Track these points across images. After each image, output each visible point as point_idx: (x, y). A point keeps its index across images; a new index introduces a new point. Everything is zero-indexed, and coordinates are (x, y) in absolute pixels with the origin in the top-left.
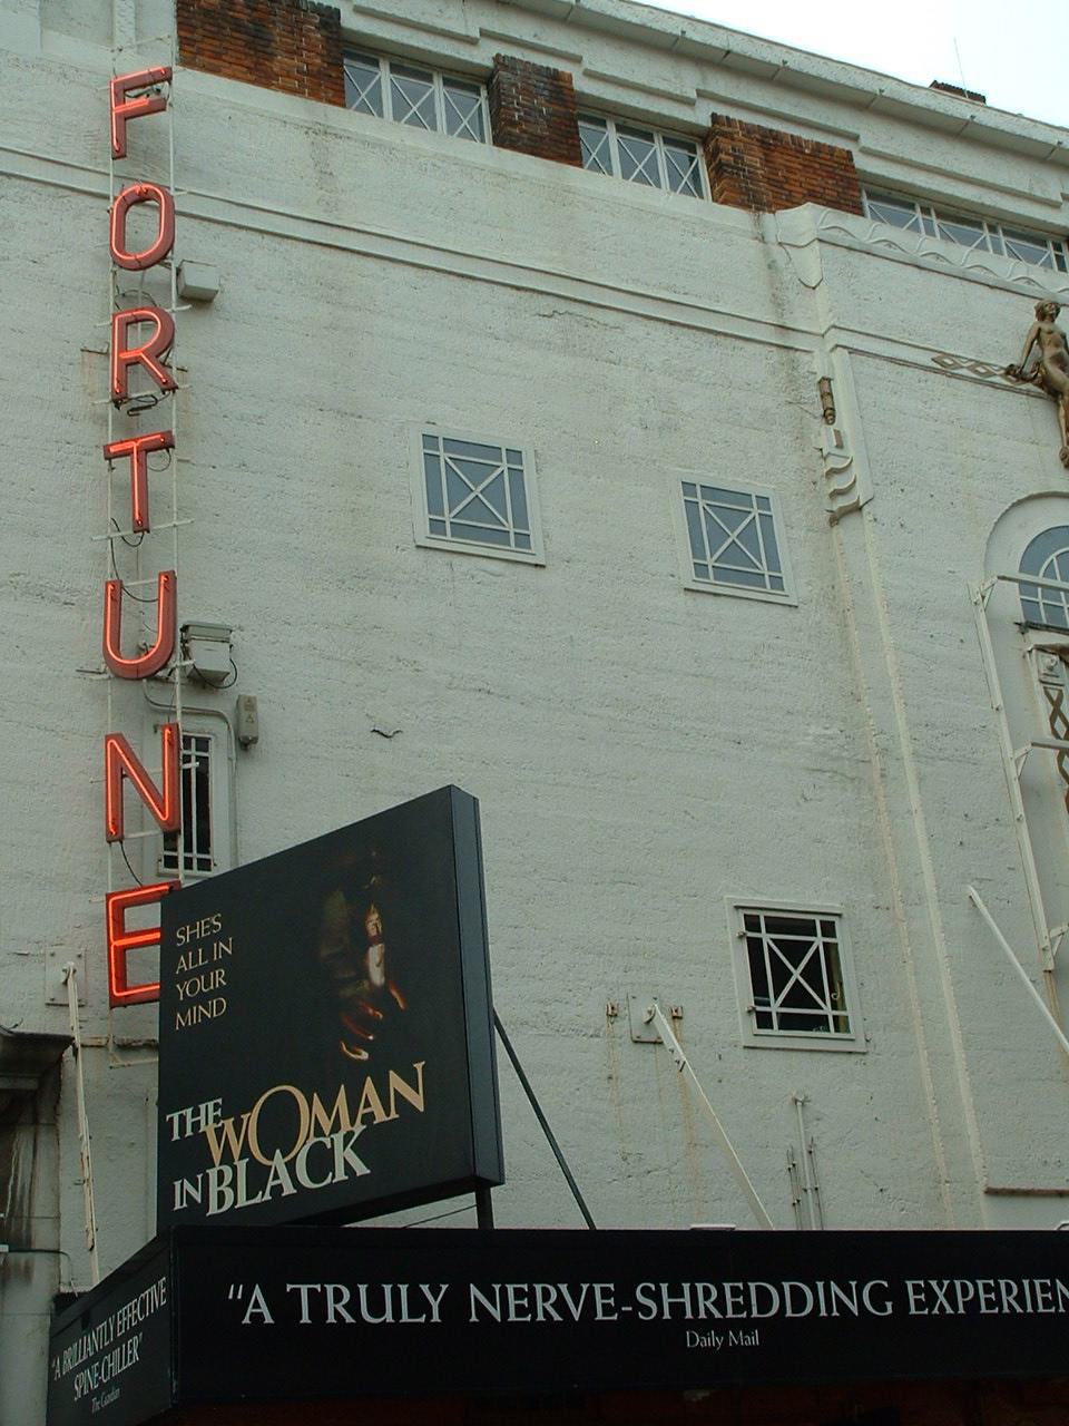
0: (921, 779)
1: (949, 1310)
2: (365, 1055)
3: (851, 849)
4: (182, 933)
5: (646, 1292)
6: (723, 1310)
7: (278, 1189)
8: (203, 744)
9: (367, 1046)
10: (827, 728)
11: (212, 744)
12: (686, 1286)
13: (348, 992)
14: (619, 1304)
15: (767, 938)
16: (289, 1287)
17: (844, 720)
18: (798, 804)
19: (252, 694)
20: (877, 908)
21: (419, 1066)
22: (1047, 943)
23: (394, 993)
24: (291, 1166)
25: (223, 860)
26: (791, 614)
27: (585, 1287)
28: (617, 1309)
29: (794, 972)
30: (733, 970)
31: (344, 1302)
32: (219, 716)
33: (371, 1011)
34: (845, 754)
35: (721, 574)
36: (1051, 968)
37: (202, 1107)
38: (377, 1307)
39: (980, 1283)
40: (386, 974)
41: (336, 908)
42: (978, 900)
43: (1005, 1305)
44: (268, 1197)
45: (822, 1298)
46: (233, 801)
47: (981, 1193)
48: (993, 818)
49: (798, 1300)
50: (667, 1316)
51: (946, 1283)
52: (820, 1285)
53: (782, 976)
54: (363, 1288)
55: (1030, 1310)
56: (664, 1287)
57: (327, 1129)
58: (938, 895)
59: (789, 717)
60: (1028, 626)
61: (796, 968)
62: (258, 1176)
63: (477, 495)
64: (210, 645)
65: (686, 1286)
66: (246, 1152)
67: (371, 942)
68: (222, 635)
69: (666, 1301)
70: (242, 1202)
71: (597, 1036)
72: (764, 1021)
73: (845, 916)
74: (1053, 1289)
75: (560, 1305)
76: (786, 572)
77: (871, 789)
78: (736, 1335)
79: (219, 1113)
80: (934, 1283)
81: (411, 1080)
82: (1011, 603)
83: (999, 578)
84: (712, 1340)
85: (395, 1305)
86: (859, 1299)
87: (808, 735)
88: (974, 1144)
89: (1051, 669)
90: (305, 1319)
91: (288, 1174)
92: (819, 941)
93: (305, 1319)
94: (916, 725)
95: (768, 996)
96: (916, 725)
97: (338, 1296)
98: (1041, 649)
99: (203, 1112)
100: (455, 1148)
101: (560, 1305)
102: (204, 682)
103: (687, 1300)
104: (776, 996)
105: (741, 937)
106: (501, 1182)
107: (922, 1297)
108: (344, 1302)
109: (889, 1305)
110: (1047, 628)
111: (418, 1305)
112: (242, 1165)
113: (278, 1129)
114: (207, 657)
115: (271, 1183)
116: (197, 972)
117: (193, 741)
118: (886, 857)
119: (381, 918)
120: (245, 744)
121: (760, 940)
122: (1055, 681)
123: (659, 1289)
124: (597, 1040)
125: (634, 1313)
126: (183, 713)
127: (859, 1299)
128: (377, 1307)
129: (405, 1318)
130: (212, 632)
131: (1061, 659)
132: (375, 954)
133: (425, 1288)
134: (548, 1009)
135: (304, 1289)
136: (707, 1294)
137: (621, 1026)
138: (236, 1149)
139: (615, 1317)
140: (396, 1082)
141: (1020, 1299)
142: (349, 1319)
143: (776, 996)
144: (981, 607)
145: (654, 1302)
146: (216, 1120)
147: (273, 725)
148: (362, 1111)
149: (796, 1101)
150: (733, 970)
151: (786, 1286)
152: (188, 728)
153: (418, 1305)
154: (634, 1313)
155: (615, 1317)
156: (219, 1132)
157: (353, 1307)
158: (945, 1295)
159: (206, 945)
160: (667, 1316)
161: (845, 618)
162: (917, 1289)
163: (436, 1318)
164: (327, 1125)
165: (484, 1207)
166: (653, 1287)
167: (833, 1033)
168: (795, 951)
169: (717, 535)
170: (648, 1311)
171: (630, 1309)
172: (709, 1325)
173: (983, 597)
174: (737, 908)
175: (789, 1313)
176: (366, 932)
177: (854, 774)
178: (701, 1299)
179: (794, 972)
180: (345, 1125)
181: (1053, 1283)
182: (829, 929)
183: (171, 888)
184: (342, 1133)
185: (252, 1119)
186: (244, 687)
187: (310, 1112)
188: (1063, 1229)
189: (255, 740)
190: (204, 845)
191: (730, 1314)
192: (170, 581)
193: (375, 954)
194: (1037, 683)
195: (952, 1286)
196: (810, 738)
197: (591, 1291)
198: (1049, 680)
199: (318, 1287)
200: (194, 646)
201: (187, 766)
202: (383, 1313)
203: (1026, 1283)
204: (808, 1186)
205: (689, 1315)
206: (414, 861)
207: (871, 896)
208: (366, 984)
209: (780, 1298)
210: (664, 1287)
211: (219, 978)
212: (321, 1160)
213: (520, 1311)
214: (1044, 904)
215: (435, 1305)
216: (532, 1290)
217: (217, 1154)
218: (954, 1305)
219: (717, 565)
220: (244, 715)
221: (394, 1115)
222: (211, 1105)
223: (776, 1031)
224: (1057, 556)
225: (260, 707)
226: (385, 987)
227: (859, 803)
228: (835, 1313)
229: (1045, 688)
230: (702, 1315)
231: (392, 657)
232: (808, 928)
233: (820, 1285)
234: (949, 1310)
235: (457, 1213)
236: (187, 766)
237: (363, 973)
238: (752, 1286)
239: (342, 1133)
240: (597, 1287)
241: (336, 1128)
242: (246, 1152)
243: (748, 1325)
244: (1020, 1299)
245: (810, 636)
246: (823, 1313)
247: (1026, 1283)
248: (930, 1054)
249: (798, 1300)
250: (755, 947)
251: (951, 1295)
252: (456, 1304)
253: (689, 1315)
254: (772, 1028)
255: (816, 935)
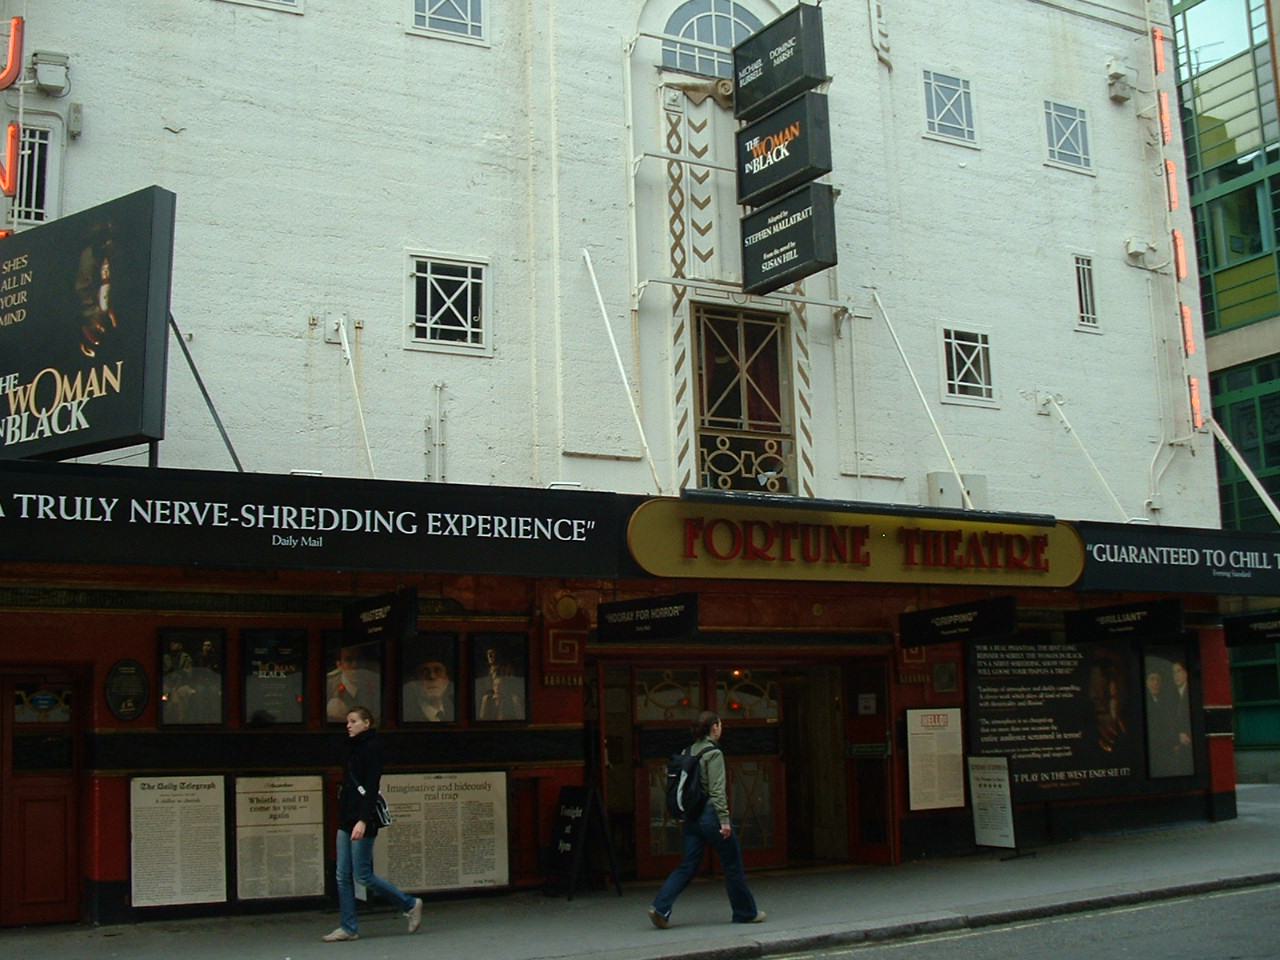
0: (561, 173)
1: (456, 533)
2: (93, 354)
3: (503, 219)
4: (7, 265)
5: (249, 510)
6: (300, 525)
7: (42, 432)
8: (44, 135)
9: (95, 348)
10: (498, 135)
11: (50, 136)
12: (276, 508)
13: (88, 313)
14: (229, 517)
15: (430, 277)
16: (16, 496)
17: (513, 129)
18: (469, 187)
19: (79, 102)
20: (516, 260)
21: (119, 364)
22: (636, 292)
23: (111, 317)
24: (49, 418)
25: (51, 214)
26: (485, 53)
27: (208, 505)
28: (227, 519)
29: (448, 302)
30: (404, 298)
31: (50, 506)
32: (60, 118)
33: (98, 327)
34: (509, 153)
35: (434, 23)
36: (636, 308)
37: (8, 377)
38: (70, 510)
39: (480, 518)
40: (109, 303)
41: (87, 258)
42: (588, 259)
43: (496, 531)
44: (37, 437)
45: (369, 521)
46: (62, 173)
47: (560, 453)
48: (612, 203)
49: (352, 520)
50: (261, 525)
51: (456, 516)
52: (368, 512)
53: (438, 302)
54: (63, 499)
55: (513, 536)
56: (261, 508)
57: (69, 399)
58: (560, 254)
59: (471, 126)
60: (662, 69)
61: (449, 297)
62: (33, 422)
63: (949, 107)
64: (52, 67)
65: (276, 508)
66: (28, 409)
67: (103, 282)
68: (62, 61)
69: (262, 516)
70: (24, 439)
71: (300, 337)
72: (421, 333)
73: (491, 265)
74: (532, 524)
75: (190, 515)
76: (485, 23)
77: (525, 178)
78: (307, 540)
79: (16, 382)
80: (448, 516)
81: (114, 371)
82: (654, 52)
83: (641, 34)
84: (290, 542)
85: (83, 509)
86: (395, 523)
87: (483, 139)
88: (560, 421)
89: (674, 101)
90: (24, 515)
91: (48, 424)
92: (469, 281)
93: (24, 515)
94: (563, 136)
95: (425, 314)
96: (563, 136)
97: (46, 502)
98: (669, 86)
99: (8, 381)
100: (134, 414)
101: (190, 515)
102: (49, 93)
103: (275, 516)
104: (433, 315)
105: (411, 276)
106: (162, 439)
107: (438, 524)
108: (50, 506)
109: (414, 527)
110: (678, 71)
111: (98, 510)
112: (25, 415)
113: (45, 398)
114: (50, 76)
115: (39, 429)
116: (12, 292)
117: (38, 133)
118: (529, 226)
119: (110, 268)
120: (73, 136)
121: (426, 278)
122: (676, 109)
123: (257, 509)
124: (299, 340)
125: (239, 523)
126: (25, 113)
127: (395, 523)
128: (70, 510)
129: (88, 518)
130: (54, 59)
131: (684, 94)
132: (104, 290)
133: (103, 500)
134: (268, 318)
135: (25, 497)
136: (290, 513)
137: (319, 332)
138: (23, 406)
139: (226, 524)
140: (107, 372)
141: (508, 529)
142: (52, 516)
143: (433, 315)
144: (628, 54)
145: (253, 516)
146: (15, 386)
147: (94, 124)
148: (88, 389)
149: (436, 387)
150: (404, 298)
151: (345, 512)
152: (27, 122)
153: (98, 510)
154: (239, 523)
155: (226, 524)
156: (15, 393)
157: (56, 509)
158: (449, 525)
159: (17, 273)
160: (261, 525)
161: (525, 57)
162: (435, 519)
163: (108, 519)
164: (70, 396)
165: (153, 454)
166: (253, 507)
167: (469, 343)
168: (450, 287)
169: (941, 105)
170: (248, 521)
171: (236, 520)
172: (289, 532)
173: (631, 46)
174: (412, 256)
175: (344, 528)
176: (100, 275)
177: (513, 168)
178: (285, 516)
179: (448, 302)
180: (79, 398)
181: (533, 521)
182: (477, 273)
183: (7, 234)
184: (77, 401)
185: (32, 387)
186: (77, 96)
187: (62, 386)
188: (553, 488)
189: (79, 134)
190: (40, 204)
191: (304, 527)
192: (20, 24)
193: (104, 290)
194: (662, 110)
195: (460, 519)
196: (484, 141)
197: (212, 508)
198: (672, 108)
199: (34, 497)
200: (41, 68)
201: (23, 152)
202: (74, 514)
203: (513, 519)
204: (437, 443)
205: (276, 526)
206: (139, 227)
207: (514, 252)
208: (98, 308)
209: (340, 519)
210: (261, 508)
211: (23, 297)
212: (65, 417)
213: (164, 517)
214: (638, 265)
215: (108, 511)
216: (173, 505)
217: (13, 408)
218: (460, 529)
219: (432, 16)
220: (73, 116)
221: (104, 393)
222: (12, 376)
223: (428, 339)
224: (698, 19)
225: (85, 110)
226: (107, 313)
227: (514, 187)
228: (376, 530)
229: (667, 114)
230: (285, 526)
231: (183, 77)
232: (463, 272)
233: (368, 512)
234: (456, 533)
235: (135, 456)
236: (23, 152)
237: (97, 302)
238: (321, 511)
239: (77, 401)
240: (216, 506)
241: (74, 399)
242: (28, 409)
243: (316, 534)
244: (508, 529)
245: (496, 69)
246: (368, 530)
247: (513, 519)
248: (538, 361)
249: (352, 520)
250: (421, 284)
251: (459, 524)
252: (122, 511)
253: (276, 526)
254: (425, 337)
255: (466, 277)
